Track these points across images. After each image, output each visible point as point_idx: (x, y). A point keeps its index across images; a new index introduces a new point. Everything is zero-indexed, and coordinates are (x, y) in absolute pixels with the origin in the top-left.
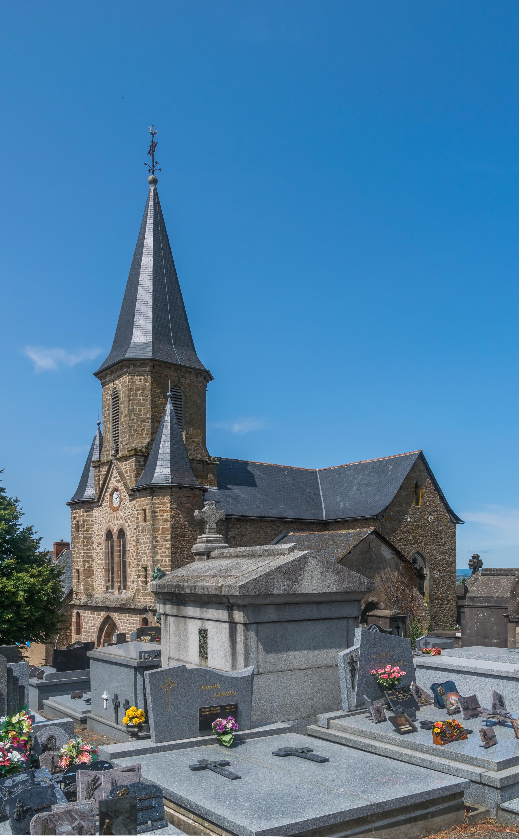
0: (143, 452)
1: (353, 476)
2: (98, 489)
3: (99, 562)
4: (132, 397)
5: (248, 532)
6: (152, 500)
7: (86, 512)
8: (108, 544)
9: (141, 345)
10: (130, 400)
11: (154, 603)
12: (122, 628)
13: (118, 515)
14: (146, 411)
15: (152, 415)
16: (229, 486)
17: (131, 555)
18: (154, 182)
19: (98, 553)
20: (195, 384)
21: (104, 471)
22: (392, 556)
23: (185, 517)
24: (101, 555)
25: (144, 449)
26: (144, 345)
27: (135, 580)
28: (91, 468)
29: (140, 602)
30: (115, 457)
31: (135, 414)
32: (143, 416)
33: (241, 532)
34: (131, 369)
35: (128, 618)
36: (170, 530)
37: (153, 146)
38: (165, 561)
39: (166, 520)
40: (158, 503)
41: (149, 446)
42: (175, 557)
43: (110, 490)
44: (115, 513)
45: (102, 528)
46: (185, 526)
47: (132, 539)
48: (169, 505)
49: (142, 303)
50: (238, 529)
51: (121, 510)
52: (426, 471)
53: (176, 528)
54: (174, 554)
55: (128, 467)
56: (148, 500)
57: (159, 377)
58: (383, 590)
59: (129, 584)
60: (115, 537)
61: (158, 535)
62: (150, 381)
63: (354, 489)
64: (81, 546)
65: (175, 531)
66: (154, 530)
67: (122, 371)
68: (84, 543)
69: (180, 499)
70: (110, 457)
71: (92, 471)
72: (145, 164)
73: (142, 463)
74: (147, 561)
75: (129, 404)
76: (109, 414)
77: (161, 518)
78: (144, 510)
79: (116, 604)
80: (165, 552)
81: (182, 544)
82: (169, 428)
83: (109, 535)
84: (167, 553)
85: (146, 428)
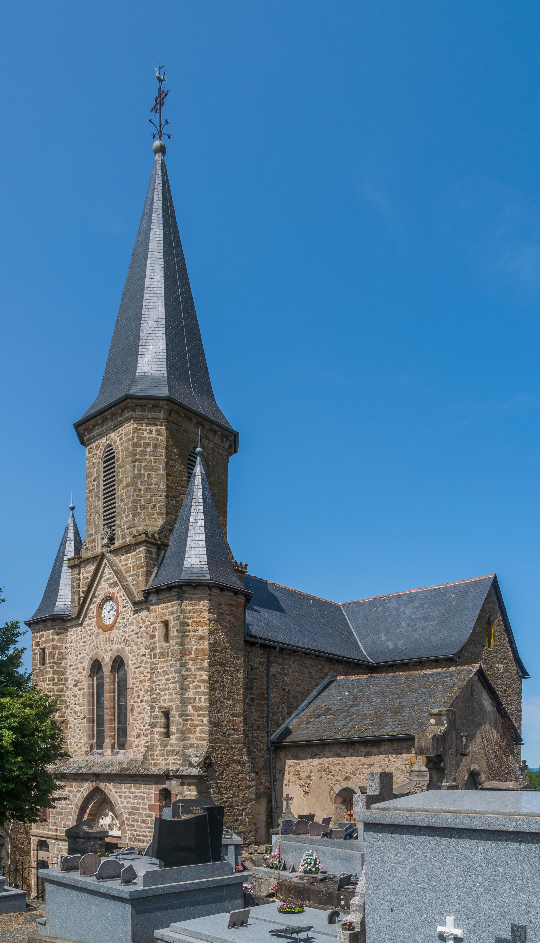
0: (156, 540)
1: (398, 609)
2: (77, 600)
3: (77, 708)
4: (138, 457)
5: (291, 670)
6: (180, 605)
7: (58, 634)
8: (93, 681)
9: (152, 379)
10: (135, 461)
11: (182, 765)
12: (121, 805)
13: (112, 636)
14: (158, 479)
15: (167, 486)
16: (256, 608)
17: (135, 694)
18: (162, 150)
19: (75, 696)
20: (220, 451)
21: (87, 573)
22: (492, 707)
23: (227, 636)
24: (81, 698)
25: (157, 536)
26: (154, 380)
27: (142, 732)
29: (155, 765)
30: (109, 549)
31: (142, 483)
32: (153, 486)
33: (282, 669)
34: (137, 413)
35: (133, 790)
36: (207, 652)
38: (200, 701)
39: (202, 638)
41: (168, 529)
42: (213, 695)
43: (98, 600)
44: (107, 633)
45: (82, 658)
46: (226, 649)
47: (137, 670)
48: (206, 615)
49: (149, 319)
50: (280, 664)
51: (118, 628)
52: (497, 604)
53: (216, 651)
54: (212, 690)
55: (132, 563)
56: (173, 606)
57: (176, 430)
58: (484, 755)
59: (130, 739)
60: (106, 669)
61: (190, 659)
62: (165, 434)
63: (404, 625)
64: (48, 685)
65: (214, 656)
66: (184, 653)
67: (122, 416)
68: (54, 680)
70: (99, 550)
72: (150, 121)
73: (154, 556)
74: (170, 700)
75: (134, 467)
76: (98, 486)
77: (194, 633)
78: (166, 624)
79: (115, 769)
80: (199, 687)
81: (222, 676)
82: (201, 500)
83: (96, 667)
84: (203, 689)
85: (158, 505)
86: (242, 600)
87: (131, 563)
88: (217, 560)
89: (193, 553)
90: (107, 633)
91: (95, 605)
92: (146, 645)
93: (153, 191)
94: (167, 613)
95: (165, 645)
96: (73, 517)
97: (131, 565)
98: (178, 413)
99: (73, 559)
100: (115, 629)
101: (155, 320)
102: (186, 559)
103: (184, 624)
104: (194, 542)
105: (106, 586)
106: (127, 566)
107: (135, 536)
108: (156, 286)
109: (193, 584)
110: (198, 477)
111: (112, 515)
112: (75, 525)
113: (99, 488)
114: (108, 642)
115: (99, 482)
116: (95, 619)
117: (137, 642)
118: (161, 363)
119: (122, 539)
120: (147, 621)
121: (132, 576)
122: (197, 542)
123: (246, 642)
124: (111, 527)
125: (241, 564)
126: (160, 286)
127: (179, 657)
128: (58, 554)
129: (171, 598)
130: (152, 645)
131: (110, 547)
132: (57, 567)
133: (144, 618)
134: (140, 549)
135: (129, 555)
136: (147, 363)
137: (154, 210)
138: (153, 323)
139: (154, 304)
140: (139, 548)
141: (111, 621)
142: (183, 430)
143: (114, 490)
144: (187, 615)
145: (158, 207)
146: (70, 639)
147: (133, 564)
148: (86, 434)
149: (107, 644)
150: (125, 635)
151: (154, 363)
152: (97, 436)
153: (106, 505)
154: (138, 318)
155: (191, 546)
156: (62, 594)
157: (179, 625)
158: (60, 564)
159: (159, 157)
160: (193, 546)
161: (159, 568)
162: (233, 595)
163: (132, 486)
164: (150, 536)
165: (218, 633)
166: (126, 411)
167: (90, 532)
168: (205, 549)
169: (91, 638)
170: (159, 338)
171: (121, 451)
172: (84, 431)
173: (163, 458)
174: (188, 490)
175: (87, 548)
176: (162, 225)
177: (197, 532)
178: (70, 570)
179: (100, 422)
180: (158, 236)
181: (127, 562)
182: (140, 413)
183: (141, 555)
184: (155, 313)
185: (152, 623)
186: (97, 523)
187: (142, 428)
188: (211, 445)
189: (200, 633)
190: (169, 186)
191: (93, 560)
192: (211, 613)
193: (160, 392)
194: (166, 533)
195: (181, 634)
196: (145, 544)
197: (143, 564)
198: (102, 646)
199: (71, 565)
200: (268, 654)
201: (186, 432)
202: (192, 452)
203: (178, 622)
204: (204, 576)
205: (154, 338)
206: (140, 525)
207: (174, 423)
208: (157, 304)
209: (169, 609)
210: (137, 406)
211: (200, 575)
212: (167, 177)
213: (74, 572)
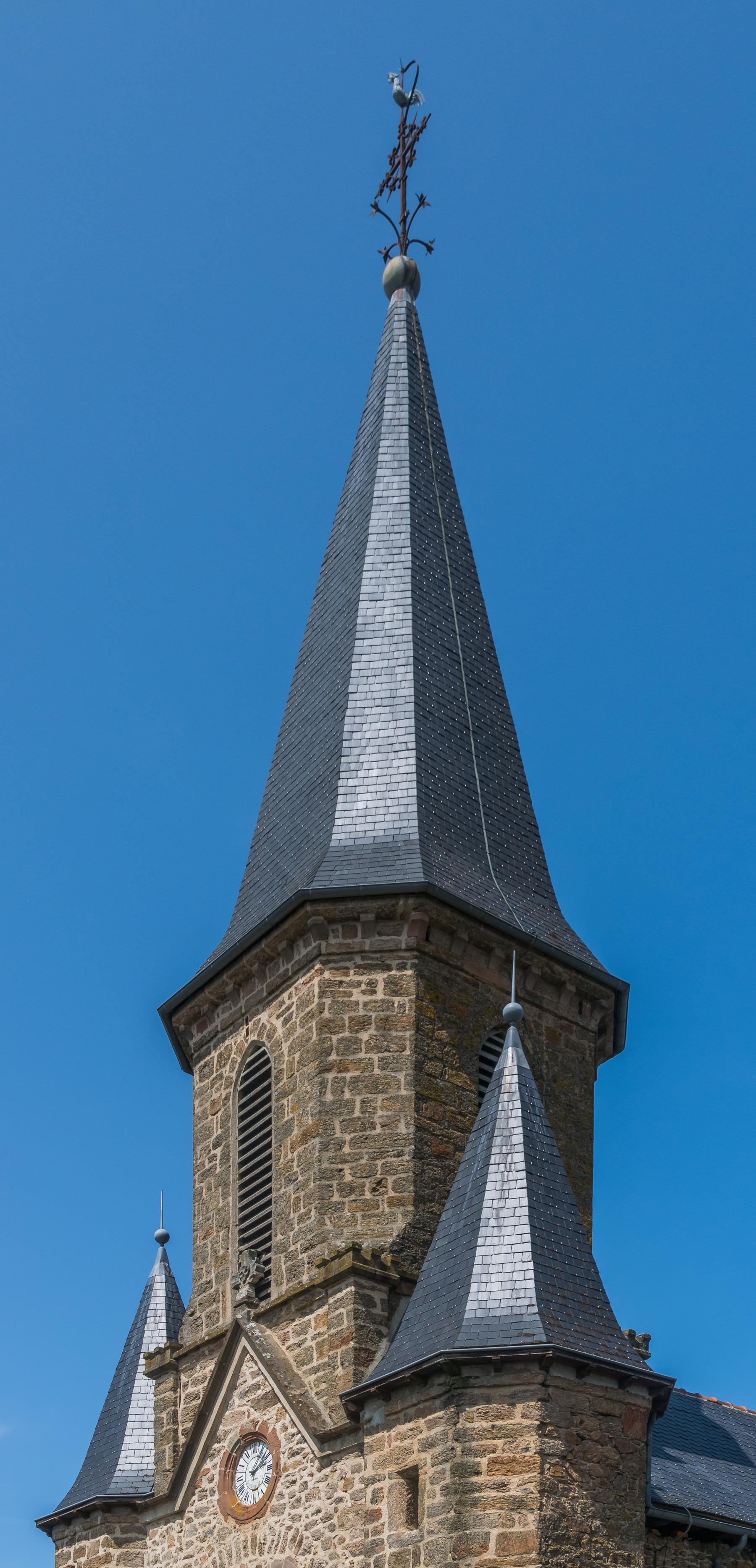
0: (383, 1267)
4: (333, 1057)
7: (119, 1543)
9: (375, 851)
13: (260, 1534)
14: (393, 1112)
15: (419, 1128)
18: (409, 279)
20: (573, 1038)
21: (196, 1383)
23: (595, 1499)
25: (386, 1257)
26: (384, 850)
28: (139, 1375)
30: (253, 1312)
31: (347, 1124)
32: (378, 1130)
34: (332, 941)
36: (534, 1543)
37: (409, 135)
39: (518, 1504)
40: (483, 1434)
41: (416, 1241)
43: (224, 1446)
48: (532, 1441)
49: (369, 703)
53: (559, 1539)
56: (431, 1426)
57: (446, 979)
62: (413, 989)
65: (555, 1553)
67: (289, 958)
69: (577, 1419)
71: (144, 1388)
73: (378, 1311)
75: (323, 1085)
76: (225, 1157)
77: (495, 1493)
78: (411, 1477)
82: (518, 1138)
85: (390, 1180)
86: (640, 1402)
87: (313, 1338)
88: (566, 1294)
89: (494, 1278)
90: (247, 1530)
91: (217, 1460)
92: (355, 1545)
93: (384, 384)
94: (415, 1447)
95: (406, 1533)
96: (165, 1259)
97: (313, 1344)
98: (452, 933)
99: (160, 1351)
100: (268, 1513)
101: (386, 702)
102: (471, 1297)
103: (463, 1471)
104: (497, 1250)
105: (245, 1408)
106: (303, 1346)
107: (324, 1263)
108: (388, 618)
109: (494, 1357)
110: (510, 1055)
111: (261, 1226)
112: (170, 1280)
113: (228, 1160)
114: (249, 1549)
115: (227, 1146)
116: (217, 1496)
117: (329, 1538)
118: (402, 809)
119: (288, 1282)
120: (357, 1480)
121: (316, 1370)
122: (505, 1249)
123: (651, 1523)
124: (259, 1255)
125: (632, 1334)
126: (400, 617)
127: (450, 1560)
128: (125, 1353)
129: (427, 1404)
130: (370, 1539)
131: (256, 1306)
132: (122, 1384)
133: (349, 1475)
134: (339, 1295)
135: (307, 1318)
136: (361, 813)
137: (383, 429)
138: (380, 710)
139: (385, 664)
140: (335, 1293)
141: (259, 1496)
142: (466, 980)
143: (269, 1157)
144: (474, 1444)
145: (396, 422)
146: (152, 1554)
147: (319, 1339)
148: (194, 1032)
149: (246, 1555)
150: (297, 1525)
151: (382, 811)
152: (223, 1030)
153: (245, 1201)
154: (338, 705)
155: (488, 1260)
156: (131, 1446)
157: (448, 1473)
158: (129, 1376)
159: (401, 298)
160: (495, 1259)
161: (392, 1341)
162: (616, 1387)
163: (318, 1135)
164: (369, 1258)
165: (569, 1490)
166: (301, 943)
167: (204, 1280)
168: (531, 1265)
169: (205, 1545)
170: (397, 747)
171: (286, 1053)
172: (189, 1023)
173: (408, 1052)
174: (479, 1117)
175: (196, 1320)
176: (407, 464)
177: (507, 1222)
178: (152, 1382)
179: (229, 988)
180: (397, 493)
181: (302, 1337)
182: (340, 940)
183: (342, 1310)
184: (384, 686)
185: (373, 1480)
186: (221, 1252)
187: (347, 979)
188: (548, 1021)
189: (512, 1493)
190: (427, 370)
191: (212, 1346)
192: (546, 1436)
193: (400, 877)
194: (416, 1251)
195: (454, 1499)
196: (352, 1280)
197: (346, 1333)
198: (234, 1561)
199: (153, 1368)
200: (713, 1559)
201: (476, 985)
202: (490, 1040)
203: (447, 1466)
204: (527, 1335)
205: (383, 749)
206: (339, 1235)
207: (440, 960)
208: (392, 663)
209: (420, 1437)
210: (331, 921)
211: (515, 1334)
212: (422, 346)
213: (161, 1387)
